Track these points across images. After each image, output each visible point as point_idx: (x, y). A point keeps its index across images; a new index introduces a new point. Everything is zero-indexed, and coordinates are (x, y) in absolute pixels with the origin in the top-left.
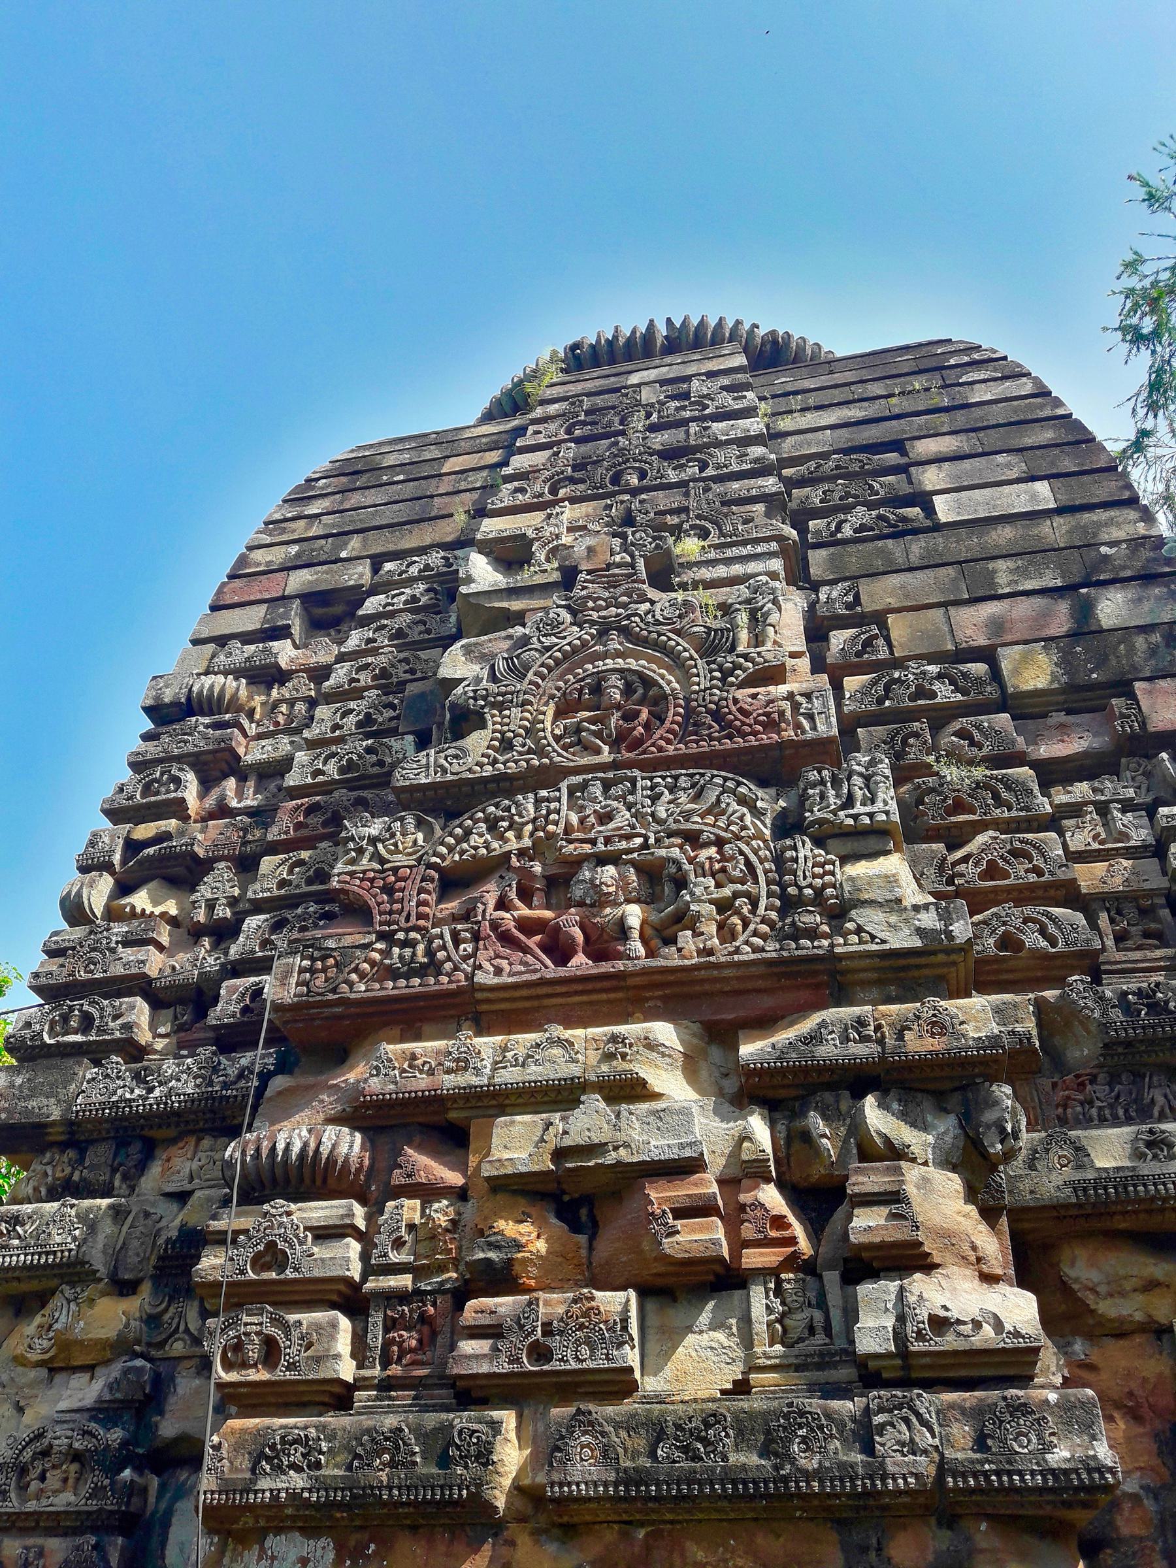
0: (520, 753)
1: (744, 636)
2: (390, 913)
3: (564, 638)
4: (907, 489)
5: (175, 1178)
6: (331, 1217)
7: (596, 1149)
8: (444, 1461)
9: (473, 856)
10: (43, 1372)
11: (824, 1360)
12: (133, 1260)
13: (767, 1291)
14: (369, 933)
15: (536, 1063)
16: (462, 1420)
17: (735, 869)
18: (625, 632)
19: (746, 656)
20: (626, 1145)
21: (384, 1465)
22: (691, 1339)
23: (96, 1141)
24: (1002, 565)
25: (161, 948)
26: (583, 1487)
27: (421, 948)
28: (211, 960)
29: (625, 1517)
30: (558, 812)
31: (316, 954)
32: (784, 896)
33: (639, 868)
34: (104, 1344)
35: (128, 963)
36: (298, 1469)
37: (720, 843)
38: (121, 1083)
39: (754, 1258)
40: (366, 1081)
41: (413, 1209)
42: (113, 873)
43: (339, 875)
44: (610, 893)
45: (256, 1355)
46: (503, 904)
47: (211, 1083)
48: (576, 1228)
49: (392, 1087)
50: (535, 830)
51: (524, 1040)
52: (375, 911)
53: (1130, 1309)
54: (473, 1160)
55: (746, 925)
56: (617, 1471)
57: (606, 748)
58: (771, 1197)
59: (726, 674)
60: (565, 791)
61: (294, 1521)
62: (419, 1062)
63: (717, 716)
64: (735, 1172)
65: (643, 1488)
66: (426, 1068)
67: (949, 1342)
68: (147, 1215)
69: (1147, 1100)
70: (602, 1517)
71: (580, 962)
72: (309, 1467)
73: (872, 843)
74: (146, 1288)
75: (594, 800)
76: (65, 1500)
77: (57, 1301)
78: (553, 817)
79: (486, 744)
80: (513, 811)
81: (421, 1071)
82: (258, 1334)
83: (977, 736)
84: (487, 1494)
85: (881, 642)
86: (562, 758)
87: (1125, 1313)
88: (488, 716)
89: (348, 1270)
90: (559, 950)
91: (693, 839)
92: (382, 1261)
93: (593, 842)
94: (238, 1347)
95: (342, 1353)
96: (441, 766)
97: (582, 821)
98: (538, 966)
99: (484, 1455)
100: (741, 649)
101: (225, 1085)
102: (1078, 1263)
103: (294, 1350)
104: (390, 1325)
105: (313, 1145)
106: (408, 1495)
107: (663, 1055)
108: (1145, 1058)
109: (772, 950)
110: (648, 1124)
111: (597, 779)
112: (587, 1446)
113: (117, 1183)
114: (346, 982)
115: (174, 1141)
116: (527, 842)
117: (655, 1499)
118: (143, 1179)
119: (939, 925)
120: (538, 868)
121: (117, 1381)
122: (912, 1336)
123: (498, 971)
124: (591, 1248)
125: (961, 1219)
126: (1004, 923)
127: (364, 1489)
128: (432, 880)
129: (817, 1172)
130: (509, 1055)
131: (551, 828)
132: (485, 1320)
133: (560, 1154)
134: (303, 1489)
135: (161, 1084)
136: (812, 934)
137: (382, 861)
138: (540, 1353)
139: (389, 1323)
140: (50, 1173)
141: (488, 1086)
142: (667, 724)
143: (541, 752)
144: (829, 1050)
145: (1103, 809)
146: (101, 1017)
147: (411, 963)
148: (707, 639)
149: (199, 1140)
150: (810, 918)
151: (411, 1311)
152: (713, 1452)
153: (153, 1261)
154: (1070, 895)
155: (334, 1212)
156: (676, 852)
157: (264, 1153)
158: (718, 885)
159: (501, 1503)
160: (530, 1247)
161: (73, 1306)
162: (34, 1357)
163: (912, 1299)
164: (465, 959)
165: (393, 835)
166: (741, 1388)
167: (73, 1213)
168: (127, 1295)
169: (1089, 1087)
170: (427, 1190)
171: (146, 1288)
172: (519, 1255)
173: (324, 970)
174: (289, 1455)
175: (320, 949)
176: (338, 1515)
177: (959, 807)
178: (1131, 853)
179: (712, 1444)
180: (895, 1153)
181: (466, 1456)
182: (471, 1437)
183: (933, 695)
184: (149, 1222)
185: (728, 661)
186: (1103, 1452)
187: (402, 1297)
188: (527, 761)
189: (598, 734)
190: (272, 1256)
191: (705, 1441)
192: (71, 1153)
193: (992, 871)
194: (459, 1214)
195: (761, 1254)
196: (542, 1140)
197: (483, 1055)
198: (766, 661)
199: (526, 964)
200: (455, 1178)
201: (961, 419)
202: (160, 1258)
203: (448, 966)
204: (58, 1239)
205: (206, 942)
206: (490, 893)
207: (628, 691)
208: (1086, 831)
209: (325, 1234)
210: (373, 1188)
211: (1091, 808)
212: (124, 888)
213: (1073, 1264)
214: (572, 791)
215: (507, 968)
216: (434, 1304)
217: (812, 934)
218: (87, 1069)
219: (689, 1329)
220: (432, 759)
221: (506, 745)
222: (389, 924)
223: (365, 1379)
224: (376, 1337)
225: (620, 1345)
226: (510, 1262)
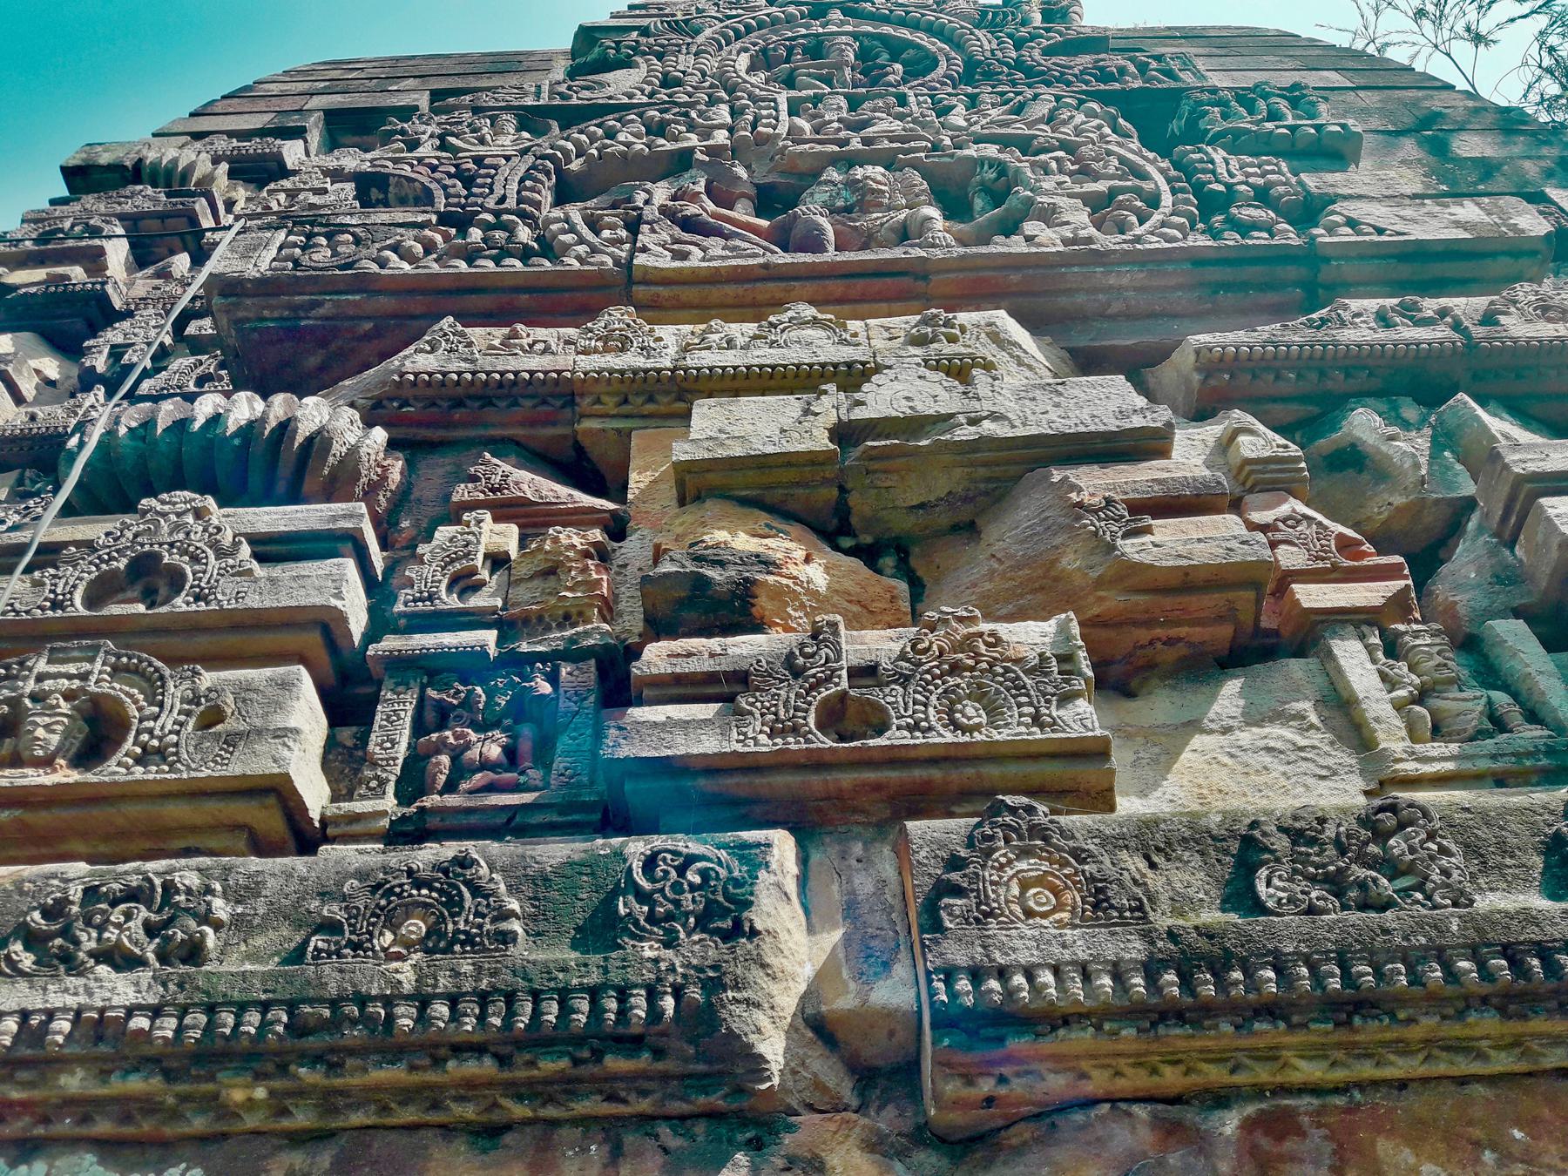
13: (1370, 649)
21: (409, 945)
26: (1047, 977)
29: (1172, 1079)
36: (123, 960)
45: (55, 739)
56: (1148, 936)
61: (85, 1119)
65: (1237, 975)
70: (1099, 1082)
72: (163, 958)
84: (737, 1018)
89: (339, 596)
95: (305, 728)
106: (482, 1018)
107: (1020, 363)
110: (1034, 399)
112: (1040, 881)
117: (1270, 1010)
127: (334, 1004)
134: (131, 1011)
139: (430, 716)
141: (673, 371)
151: (490, 694)
152: (1420, 887)
159: (773, 1048)
170: (536, 514)
172: (771, 579)
174: (101, 928)
176: (238, 1095)
179: (1410, 870)
181: (669, 917)
182: (681, 870)
187: (469, 666)
191: (1393, 869)
210: (405, 524)
216: (553, 679)
223: (357, 818)
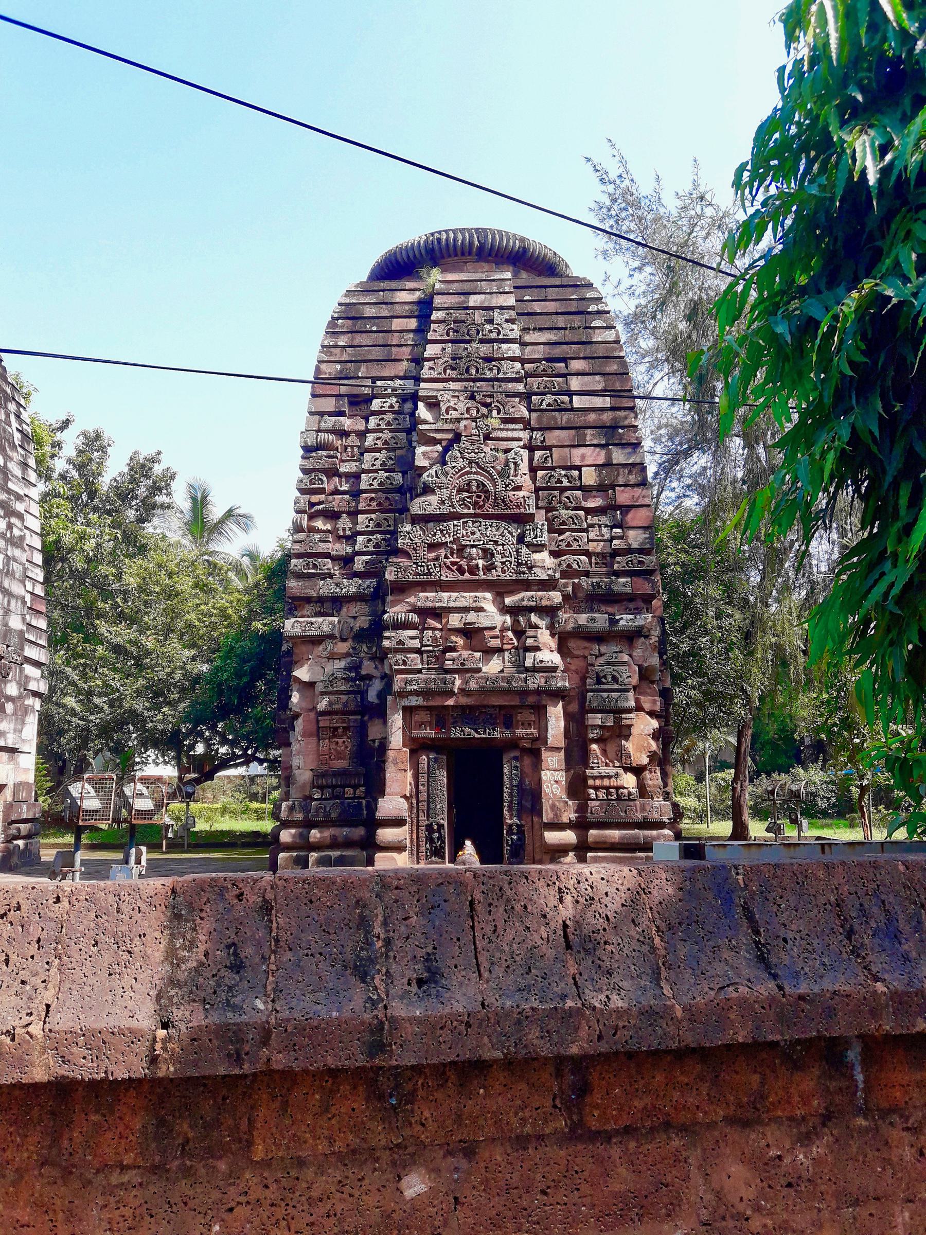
1: (512, 472)
4: (565, 387)
7: (472, 624)
8: (445, 684)
11: (518, 667)
16: (448, 676)
18: (477, 463)
24: (589, 432)
37: (503, 545)
39: (505, 647)
46: (446, 557)
51: (455, 595)
53: (580, 653)
54: (444, 621)
58: (510, 634)
59: (507, 486)
63: (503, 501)
67: (543, 665)
71: (467, 574)
73: (540, 548)
76: (343, 688)
85: (549, 459)
86: (460, 510)
91: (496, 542)
99: (453, 683)
100: (511, 478)
101: (364, 589)
104: (428, 657)
109: (514, 577)
116: (452, 539)
120: (455, 547)
129: (520, 629)
133: (465, 624)
136: (524, 573)
138: (463, 664)
143: (453, 506)
144: (525, 603)
145: (600, 526)
150: (524, 569)
154: (587, 553)
156: (491, 547)
166: (502, 671)
171: (350, 640)
177: (564, 523)
178: (604, 541)
180: (536, 627)
183: (561, 482)
186: (567, 684)
187: (430, 651)
192: (319, 604)
193: (569, 545)
201: (587, 350)
206: (442, 552)
207: (478, 487)
209: (412, 638)
212: (311, 517)
217: (524, 573)
221: (443, 502)
224: (425, 659)
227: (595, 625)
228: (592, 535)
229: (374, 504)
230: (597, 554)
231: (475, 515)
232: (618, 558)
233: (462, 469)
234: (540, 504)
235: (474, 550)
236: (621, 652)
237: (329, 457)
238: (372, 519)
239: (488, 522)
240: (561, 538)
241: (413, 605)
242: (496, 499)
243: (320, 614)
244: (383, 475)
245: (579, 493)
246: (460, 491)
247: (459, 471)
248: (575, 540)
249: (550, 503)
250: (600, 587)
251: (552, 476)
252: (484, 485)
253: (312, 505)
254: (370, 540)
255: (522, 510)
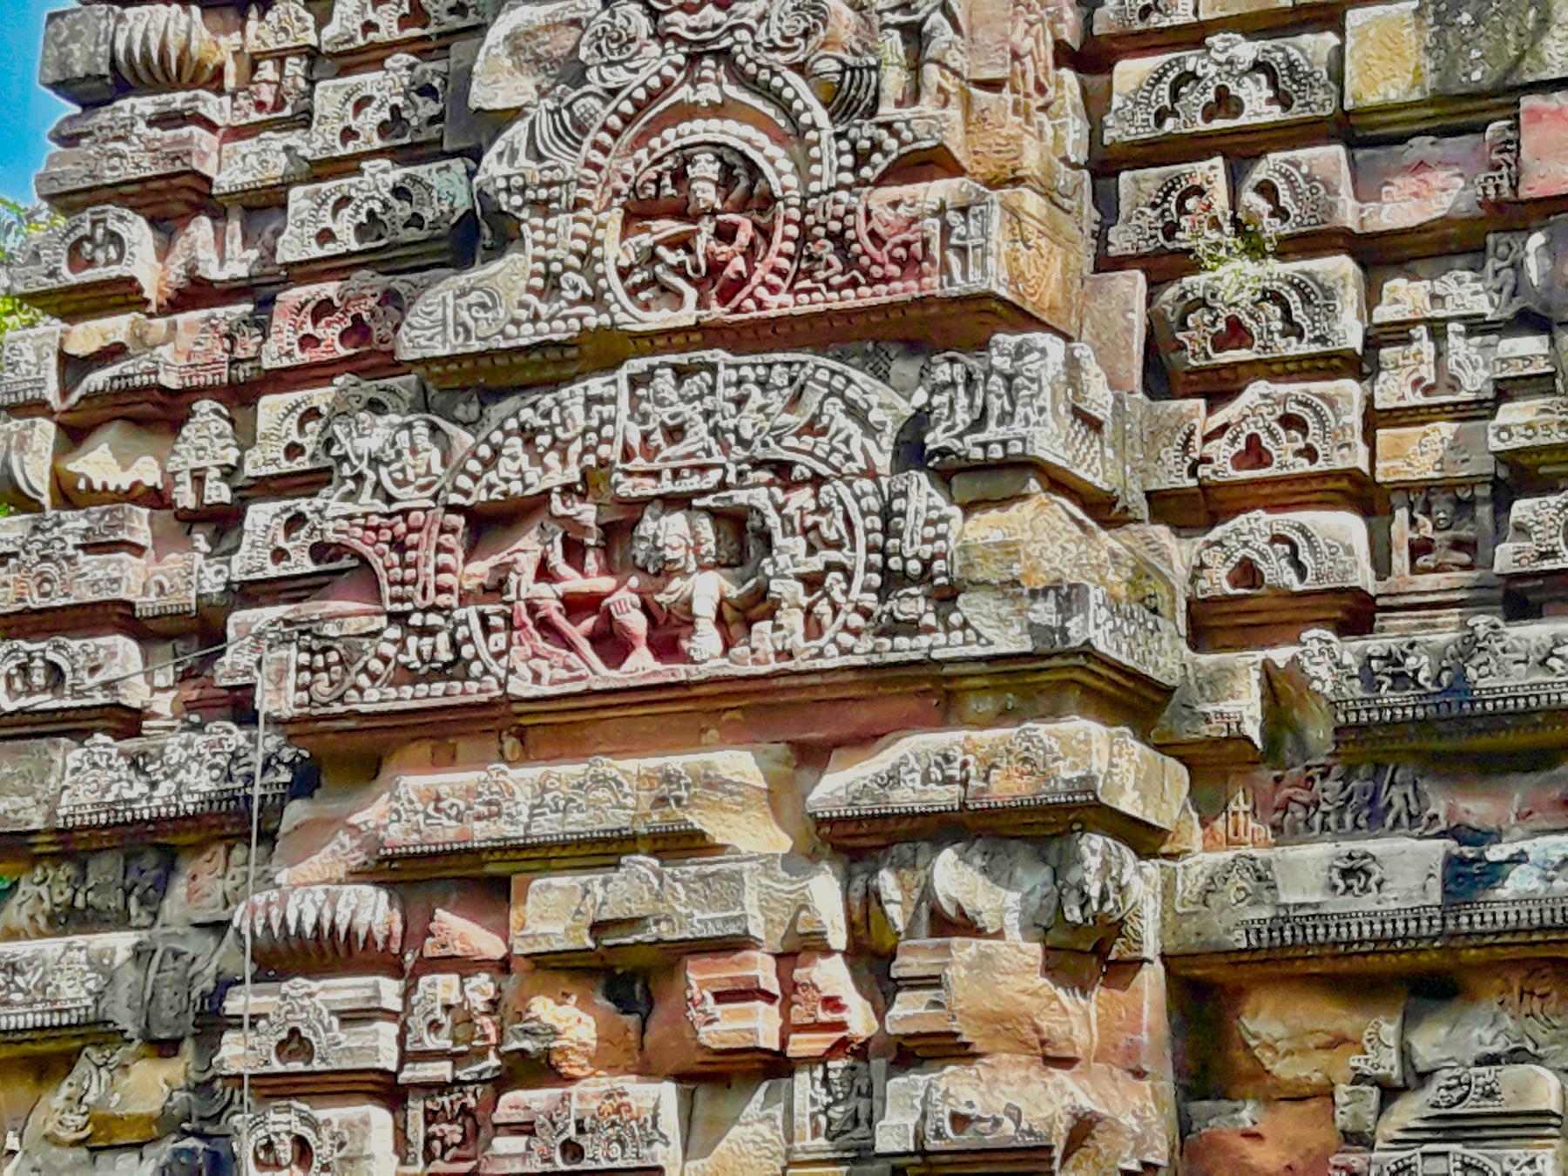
0: (572, 304)
1: (894, 80)
2: (403, 583)
3: (636, 71)
5: (206, 902)
6: (350, 1000)
7: (633, 923)
9: (505, 494)
10: (83, 1153)
12: (166, 1015)
13: (813, 1080)
14: (377, 614)
15: (579, 808)
17: (830, 525)
19: (888, 126)
20: (668, 920)
22: (736, 1131)
23: (99, 850)
25: (138, 550)
27: (443, 639)
28: (209, 573)
30: (612, 421)
31: (316, 645)
32: (885, 571)
33: (714, 514)
34: (151, 1120)
35: (95, 583)
38: (114, 775)
39: (801, 1045)
40: (385, 828)
41: (449, 987)
42: (50, 414)
43: (334, 519)
44: (676, 561)
46: (544, 572)
47: (230, 778)
48: (625, 1005)
49: (416, 837)
50: (586, 450)
52: (384, 582)
55: (836, 610)
57: (691, 294)
59: (861, 159)
60: (624, 385)
62: (443, 805)
64: (793, 945)
66: (454, 812)
67: (967, 1140)
68: (177, 955)
69: (1383, 803)
73: (1005, 483)
74: (188, 1047)
75: (660, 402)
77: (82, 1067)
78: (607, 431)
79: (523, 284)
80: (556, 418)
81: (449, 817)
82: (289, 1133)
83: (1285, 199)
87: (1302, 1074)
88: (525, 228)
90: (611, 643)
92: (418, 1047)
93: (656, 475)
94: (269, 1147)
96: (464, 325)
97: (646, 437)
98: (585, 671)
100: (886, 111)
102: (1262, 1015)
103: (326, 1150)
104: (430, 1117)
105: (327, 914)
107: (731, 793)
108: (1388, 746)
109: (864, 650)
111: (663, 365)
113: (133, 910)
114: (355, 687)
115: (199, 849)
116: (573, 474)
118: (167, 902)
119: (1054, 620)
121: (167, 1165)
122: (930, 1133)
123: (537, 677)
124: (643, 1031)
125: (1024, 998)
126: (1246, 544)
128: (454, 531)
130: (548, 797)
131: (604, 450)
132: (519, 1117)
133: (597, 928)
135: (167, 776)
136: (912, 628)
137: (390, 499)
140: (45, 896)
142: (775, 248)
143: (595, 299)
144: (906, 797)
145: (1437, 330)
146: (74, 671)
147: (433, 660)
148: (841, 83)
149: (230, 849)
153: (191, 1017)
155: (361, 993)
157: (275, 924)
158: (812, 550)
160: (569, 1034)
161: (103, 1071)
162: (70, 1136)
163: (936, 1095)
164: (498, 656)
165: (399, 454)
167: (82, 956)
168: (168, 1057)
169: (1318, 784)
173: (327, 668)
175: (318, 637)
177: (1236, 333)
183: (1235, 107)
184: (180, 964)
185: (865, 131)
187: (442, 1087)
188: (580, 317)
189: (679, 269)
190: (296, 1043)
192: (68, 870)
193: (1255, 453)
194: (499, 990)
195: (810, 1041)
196: (578, 912)
197: (519, 797)
198: (916, 139)
199: (569, 668)
200: (492, 946)
202: (197, 1015)
203: (476, 668)
204: (70, 994)
205: (201, 541)
206: (527, 548)
207: (726, 181)
208: (1405, 372)
209: (352, 1017)
211: (1422, 330)
212: (74, 434)
213: (1256, 1014)
214: (634, 382)
215: (546, 674)
217: (912, 628)
218: (68, 750)
219: (735, 1120)
220: (450, 312)
221: (551, 285)
222: (401, 600)
224: (417, 1131)
225: (650, 1143)
226: (548, 1052)
227: (1368, 903)
228: (1393, 389)
229: (330, 332)
230: (1421, 494)
231: (708, 334)
232: (1521, 509)
233: (653, 96)
234: (1121, 241)
235: (675, 524)
236: (1517, 1056)
237: (165, 120)
238: (313, 413)
239: (750, 366)
240: (1218, 419)
241: (373, 842)
242: (805, 236)
243: (68, 919)
244: (381, 176)
245: (1330, 157)
246: (638, 213)
247: (640, 107)
248: (1288, 421)
249: (1171, 230)
250: (1401, 679)
251: (1190, 77)
252: (753, 169)
253: (72, 366)
254: (297, 521)
255: (933, 284)
